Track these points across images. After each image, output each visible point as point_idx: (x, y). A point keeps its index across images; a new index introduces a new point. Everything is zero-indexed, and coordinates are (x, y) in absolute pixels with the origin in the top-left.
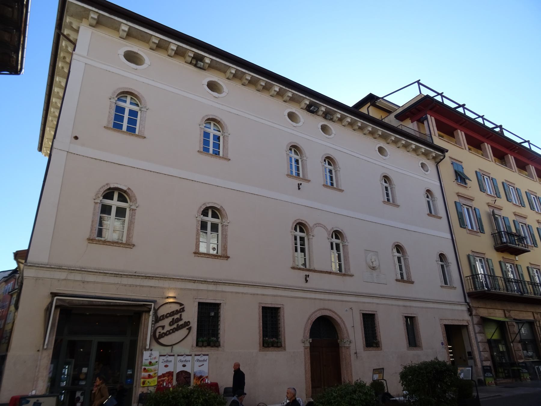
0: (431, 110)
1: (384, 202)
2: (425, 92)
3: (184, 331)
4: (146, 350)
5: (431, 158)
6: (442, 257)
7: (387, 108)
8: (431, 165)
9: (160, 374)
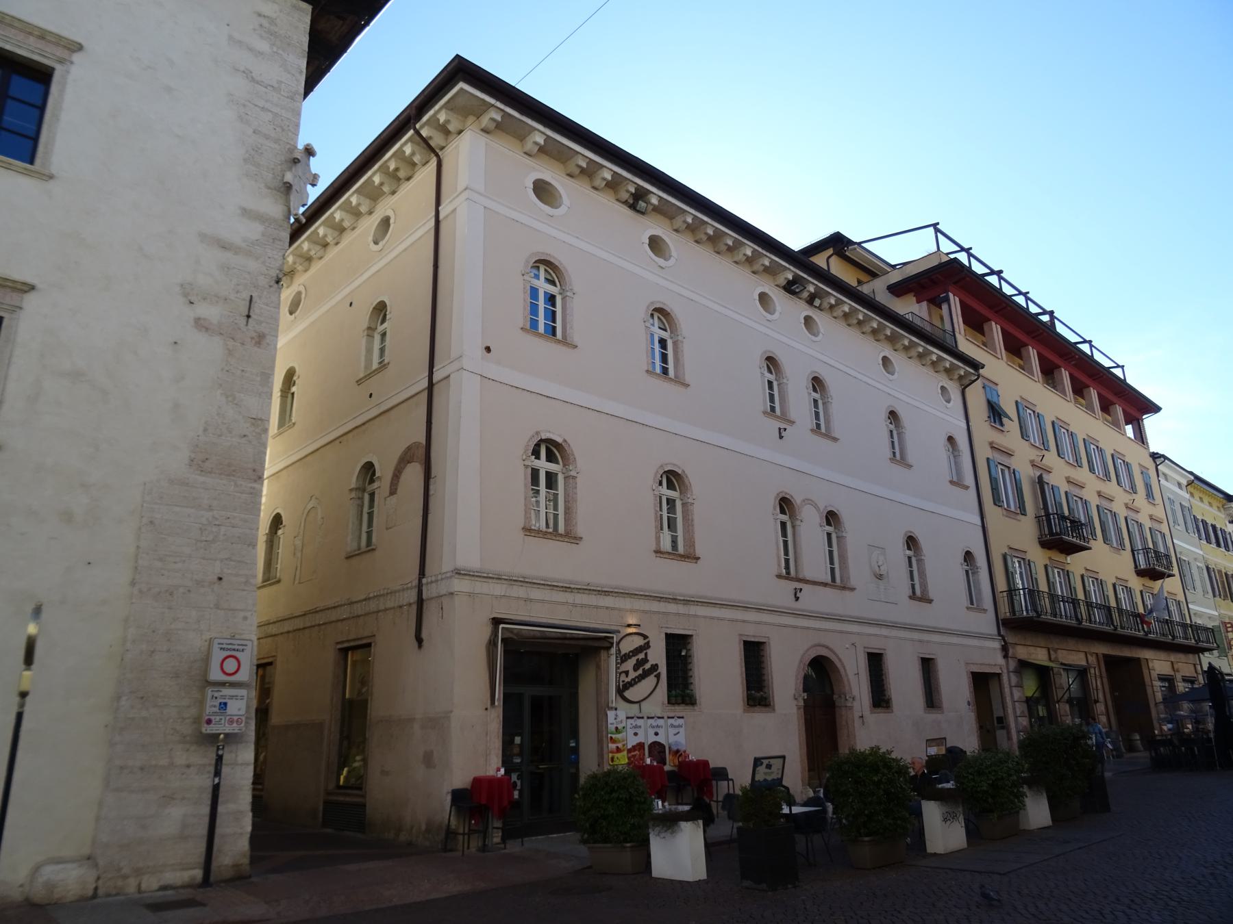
0: (955, 283)
1: (812, 430)
2: (946, 247)
3: (651, 680)
4: (611, 709)
5: (956, 377)
6: (968, 556)
7: (870, 268)
8: (954, 390)
9: (629, 746)
